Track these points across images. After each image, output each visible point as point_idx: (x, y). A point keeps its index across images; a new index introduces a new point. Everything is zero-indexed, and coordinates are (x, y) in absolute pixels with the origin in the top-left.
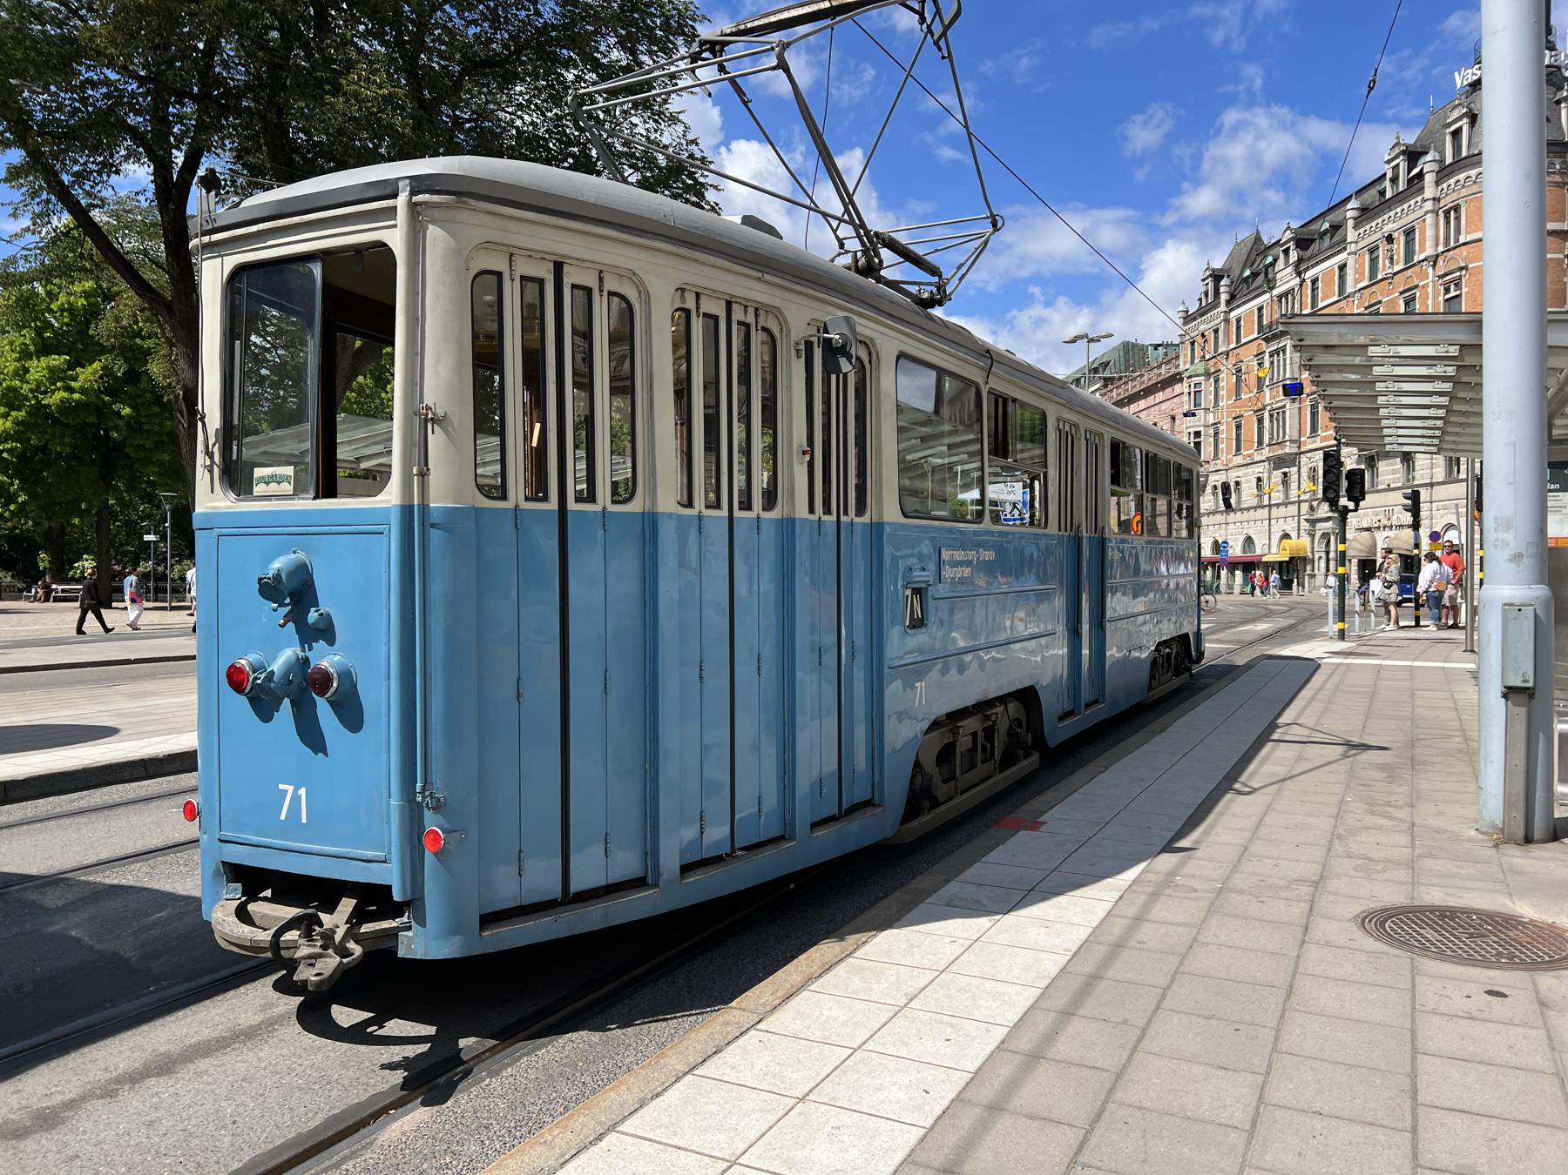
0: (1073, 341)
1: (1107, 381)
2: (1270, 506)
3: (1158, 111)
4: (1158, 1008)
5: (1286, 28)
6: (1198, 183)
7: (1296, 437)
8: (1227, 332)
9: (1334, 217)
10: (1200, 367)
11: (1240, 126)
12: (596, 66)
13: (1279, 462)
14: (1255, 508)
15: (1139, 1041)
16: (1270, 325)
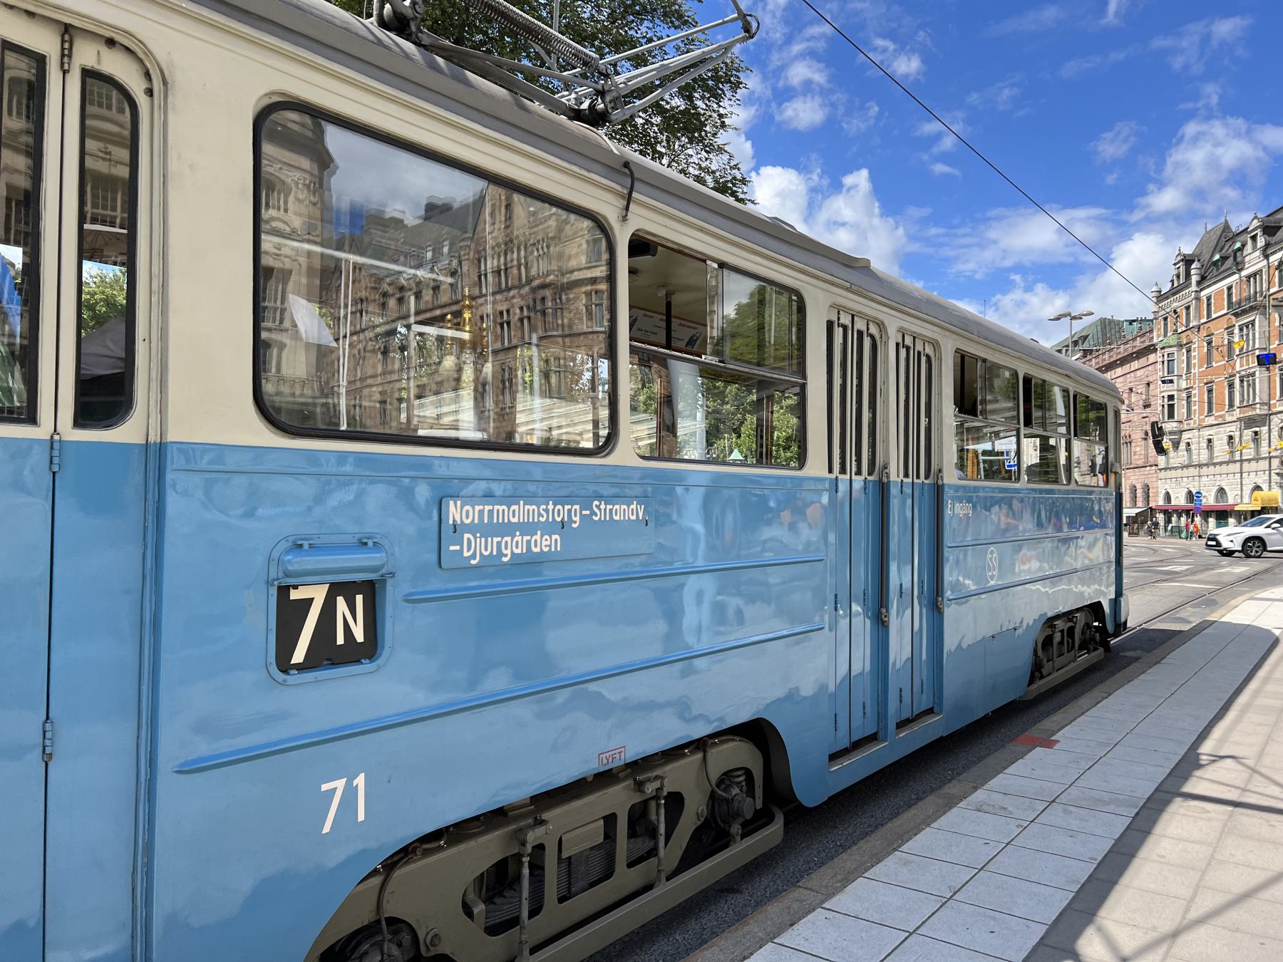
0: (1058, 319)
1: (1086, 353)
2: (1241, 461)
3: (1125, 128)
5: (1240, 52)
6: (1162, 185)
7: (1266, 400)
8: (1198, 309)
10: (1172, 339)
11: (1196, 139)
13: (1250, 422)
14: (1227, 463)
16: (1239, 303)
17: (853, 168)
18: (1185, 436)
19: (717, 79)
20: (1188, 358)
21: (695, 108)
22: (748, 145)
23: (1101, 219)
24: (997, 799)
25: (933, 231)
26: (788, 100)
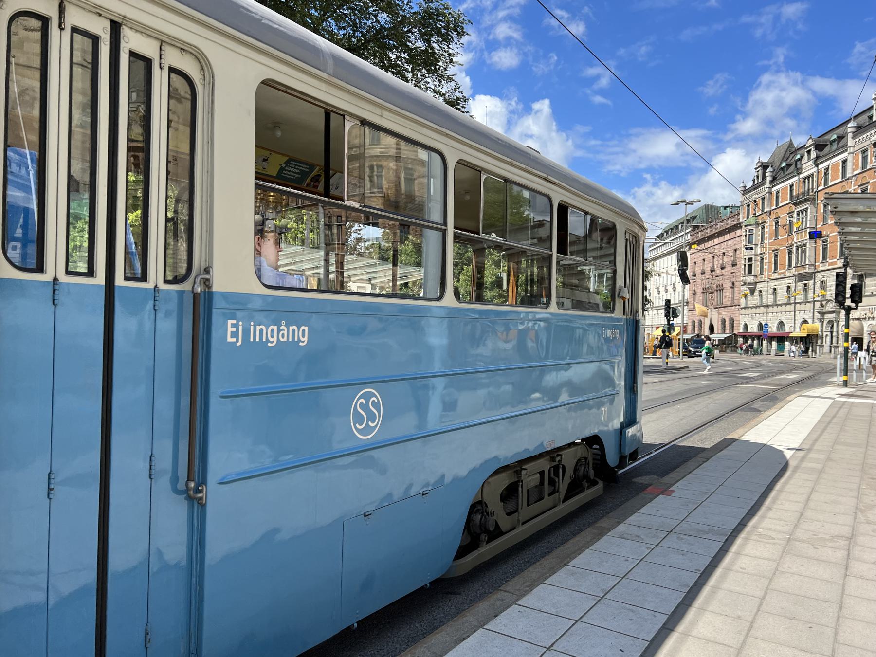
1: (695, 228)
3: (721, 77)
4: (758, 610)
5: (800, 26)
6: (746, 115)
8: (770, 199)
9: (840, 131)
10: (752, 220)
11: (769, 86)
12: (408, 50)
13: (801, 277)
14: (786, 304)
15: (749, 630)
16: (798, 196)
17: (538, 98)
18: (759, 286)
19: (447, 27)
20: (762, 233)
21: (432, 48)
22: (468, 79)
23: (705, 138)
24: (634, 530)
25: (593, 142)
26: (495, 50)
